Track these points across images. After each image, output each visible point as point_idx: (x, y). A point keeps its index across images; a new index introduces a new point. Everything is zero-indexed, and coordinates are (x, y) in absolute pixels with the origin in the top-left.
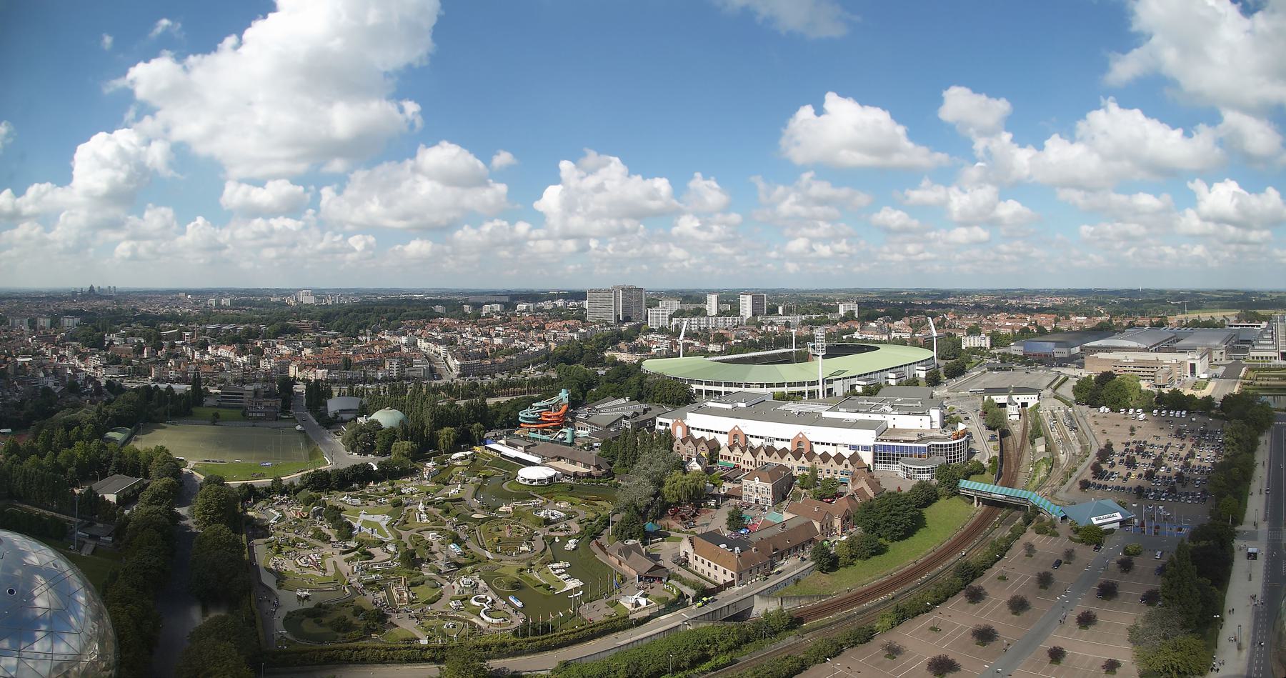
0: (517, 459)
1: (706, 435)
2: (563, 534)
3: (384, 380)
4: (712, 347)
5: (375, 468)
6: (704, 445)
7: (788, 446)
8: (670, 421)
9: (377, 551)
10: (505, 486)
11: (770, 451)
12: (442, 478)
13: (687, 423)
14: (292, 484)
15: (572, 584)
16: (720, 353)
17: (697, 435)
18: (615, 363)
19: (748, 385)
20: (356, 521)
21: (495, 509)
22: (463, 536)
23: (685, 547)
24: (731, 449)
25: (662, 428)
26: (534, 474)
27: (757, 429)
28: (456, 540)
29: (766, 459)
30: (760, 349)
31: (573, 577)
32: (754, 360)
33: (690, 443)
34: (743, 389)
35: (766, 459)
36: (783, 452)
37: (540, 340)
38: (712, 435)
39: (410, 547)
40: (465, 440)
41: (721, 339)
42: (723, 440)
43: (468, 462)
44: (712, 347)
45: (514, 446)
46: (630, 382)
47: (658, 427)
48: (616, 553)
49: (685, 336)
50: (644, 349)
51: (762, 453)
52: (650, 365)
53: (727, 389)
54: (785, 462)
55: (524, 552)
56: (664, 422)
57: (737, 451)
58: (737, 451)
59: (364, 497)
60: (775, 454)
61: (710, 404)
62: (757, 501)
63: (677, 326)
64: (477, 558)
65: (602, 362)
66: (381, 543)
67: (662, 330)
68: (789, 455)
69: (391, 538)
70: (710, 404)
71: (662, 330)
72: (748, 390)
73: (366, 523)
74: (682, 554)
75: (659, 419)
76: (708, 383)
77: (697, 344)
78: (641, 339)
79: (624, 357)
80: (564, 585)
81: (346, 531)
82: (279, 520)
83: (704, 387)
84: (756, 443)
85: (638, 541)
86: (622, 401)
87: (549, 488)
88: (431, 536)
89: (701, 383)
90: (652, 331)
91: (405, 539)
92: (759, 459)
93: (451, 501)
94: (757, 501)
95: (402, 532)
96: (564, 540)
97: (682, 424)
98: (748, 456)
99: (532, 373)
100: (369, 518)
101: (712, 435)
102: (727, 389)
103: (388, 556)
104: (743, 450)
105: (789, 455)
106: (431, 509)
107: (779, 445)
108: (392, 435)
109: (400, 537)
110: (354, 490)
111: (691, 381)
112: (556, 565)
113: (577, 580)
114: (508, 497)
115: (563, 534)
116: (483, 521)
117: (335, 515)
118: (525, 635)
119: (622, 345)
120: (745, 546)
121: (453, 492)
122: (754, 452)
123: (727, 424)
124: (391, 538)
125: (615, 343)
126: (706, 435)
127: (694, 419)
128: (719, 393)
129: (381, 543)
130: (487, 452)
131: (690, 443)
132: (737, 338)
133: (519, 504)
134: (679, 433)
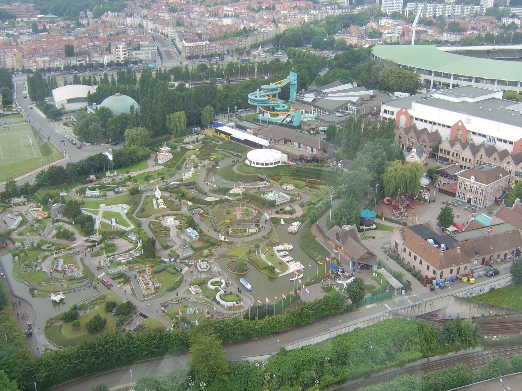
0: (246, 142)
1: (428, 127)
2: (288, 216)
3: (110, 64)
4: (445, 37)
5: (110, 157)
6: (425, 137)
7: (510, 148)
8: (396, 110)
9: (119, 242)
10: (235, 169)
11: (491, 151)
12: (177, 163)
13: (411, 112)
14: (27, 185)
15: (294, 266)
16: (453, 44)
17: (420, 126)
18: (343, 46)
19: (478, 80)
20: (96, 213)
21: (225, 191)
22: (197, 219)
23: (396, 238)
24: (452, 143)
25: (388, 116)
26: (264, 156)
27: (480, 126)
28: (192, 224)
29: (485, 159)
30: (498, 43)
31: (295, 259)
32: (487, 54)
33: (412, 133)
34: (473, 83)
35: (485, 159)
36: (504, 154)
37: (268, 21)
38: (435, 128)
39: (151, 235)
40: (196, 122)
41: (455, 28)
42: (445, 133)
43: (200, 145)
44: (445, 37)
45: (243, 128)
46: (356, 66)
47: (382, 114)
48: (333, 238)
49: (419, 23)
50: (376, 34)
51: (482, 152)
52: (381, 52)
53: (456, 82)
54: (504, 165)
55: (252, 234)
56: (390, 109)
57: (458, 147)
58: (458, 147)
59: (102, 188)
60: (495, 155)
61: (436, 96)
62: (469, 200)
63: (411, 12)
64: (213, 241)
65: (330, 45)
66: (122, 234)
67: (395, 16)
68: (509, 159)
69: (132, 227)
70: (436, 96)
71: (395, 16)
72: (477, 85)
73: (108, 215)
74: (393, 244)
75: (384, 107)
76: (437, 74)
77: (430, 32)
78: (372, 25)
79: (352, 40)
80: (287, 268)
81: (86, 225)
82: (21, 224)
83: (432, 78)
84: (478, 140)
85: (354, 227)
86: (349, 86)
87: (275, 173)
88: (170, 221)
89: (430, 73)
90: (385, 15)
91: (145, 227)
92: (478, 158)
93: (186, 185)
94: (469, 200)
95: (142, 220)
96: (289, 222)
97: (406, 114)
98: (467, 153)
99: (261, 56)
100: (108, 210)
101: (435, 128)
102: (456, 82)
103: (131, 246)
104: (464, 147)
105: (509, 159)
106: (167, 194)
107: (501, 146)
108: (124, 121)
109: (139, 225)
110: (91, 181)
111: (420, 70)
112: (280, 247)
113: (298, 263)
114: (236, 179)
115: (288, 216)
116: (217, 202)
117: (73, 211)
118: (253, 319)
119: (353, 28)
120: (450, 242)
121: (188, 175)
122: (475, 149)
123: (450, 118)
124: (132, 227)
125: (346, 26)
126: (428, 127)
127: (420, 111)
128: (448, 85)
129: (122, 234)
130: (218, 135)
131: (412, 133)
132: (473, 29)
133: (248, 186)
134: (403, 121)
